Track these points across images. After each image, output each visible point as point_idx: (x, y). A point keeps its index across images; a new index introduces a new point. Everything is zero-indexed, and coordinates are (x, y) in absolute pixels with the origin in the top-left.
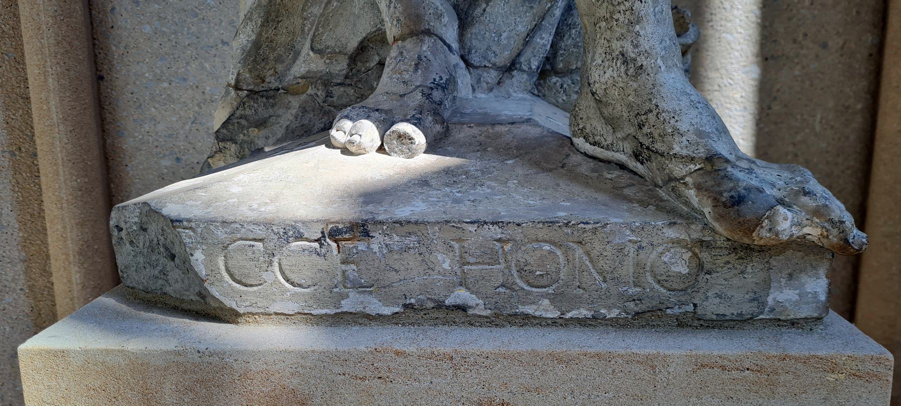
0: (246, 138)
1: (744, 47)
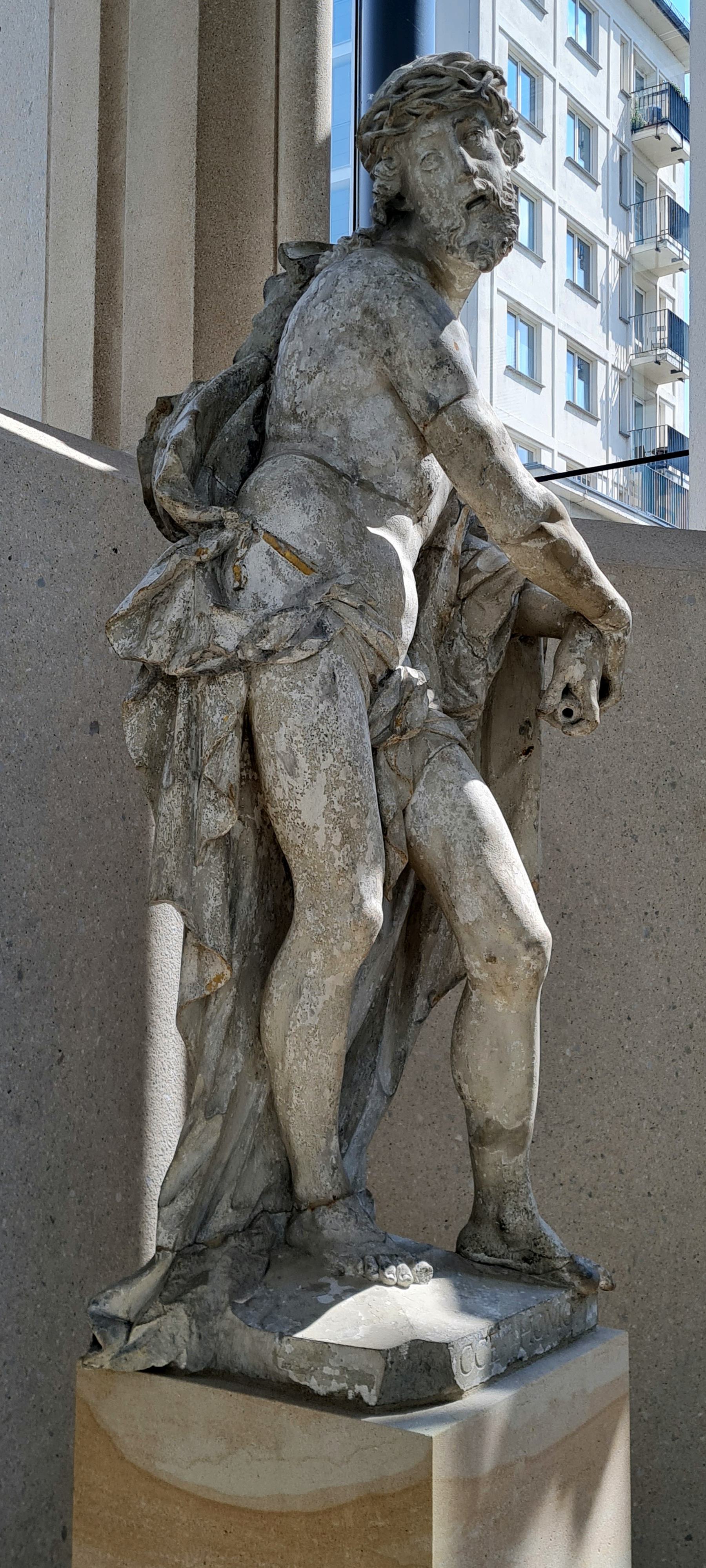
0: (194, 1296)
1: (178, 1107)
